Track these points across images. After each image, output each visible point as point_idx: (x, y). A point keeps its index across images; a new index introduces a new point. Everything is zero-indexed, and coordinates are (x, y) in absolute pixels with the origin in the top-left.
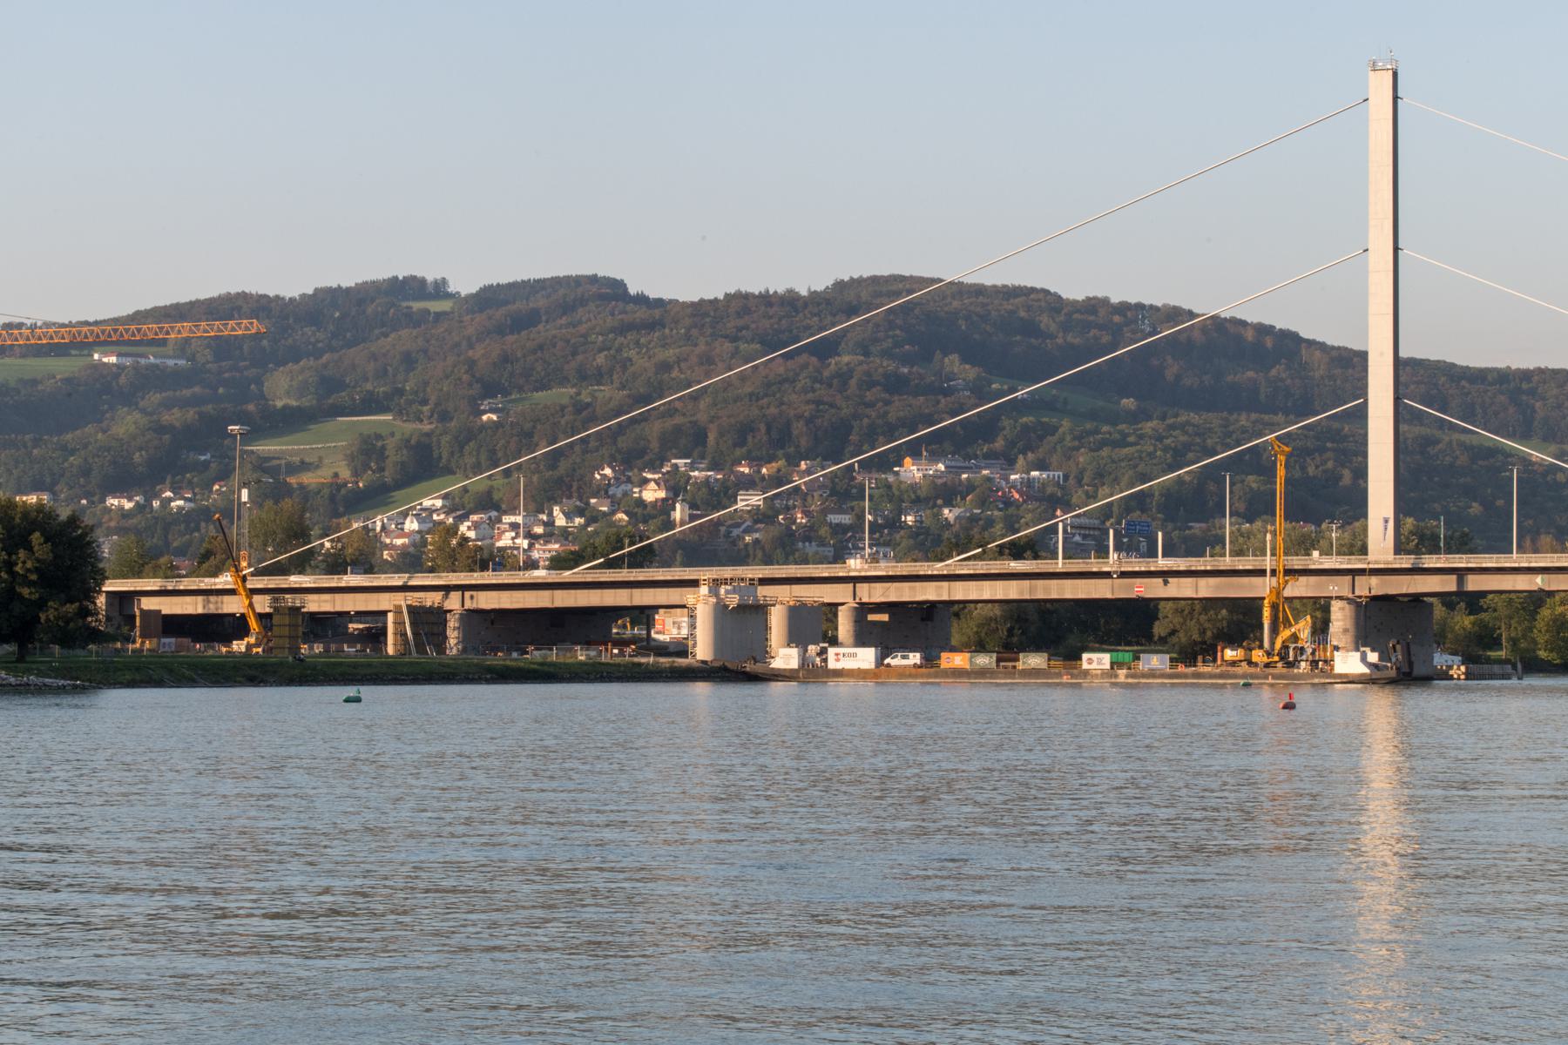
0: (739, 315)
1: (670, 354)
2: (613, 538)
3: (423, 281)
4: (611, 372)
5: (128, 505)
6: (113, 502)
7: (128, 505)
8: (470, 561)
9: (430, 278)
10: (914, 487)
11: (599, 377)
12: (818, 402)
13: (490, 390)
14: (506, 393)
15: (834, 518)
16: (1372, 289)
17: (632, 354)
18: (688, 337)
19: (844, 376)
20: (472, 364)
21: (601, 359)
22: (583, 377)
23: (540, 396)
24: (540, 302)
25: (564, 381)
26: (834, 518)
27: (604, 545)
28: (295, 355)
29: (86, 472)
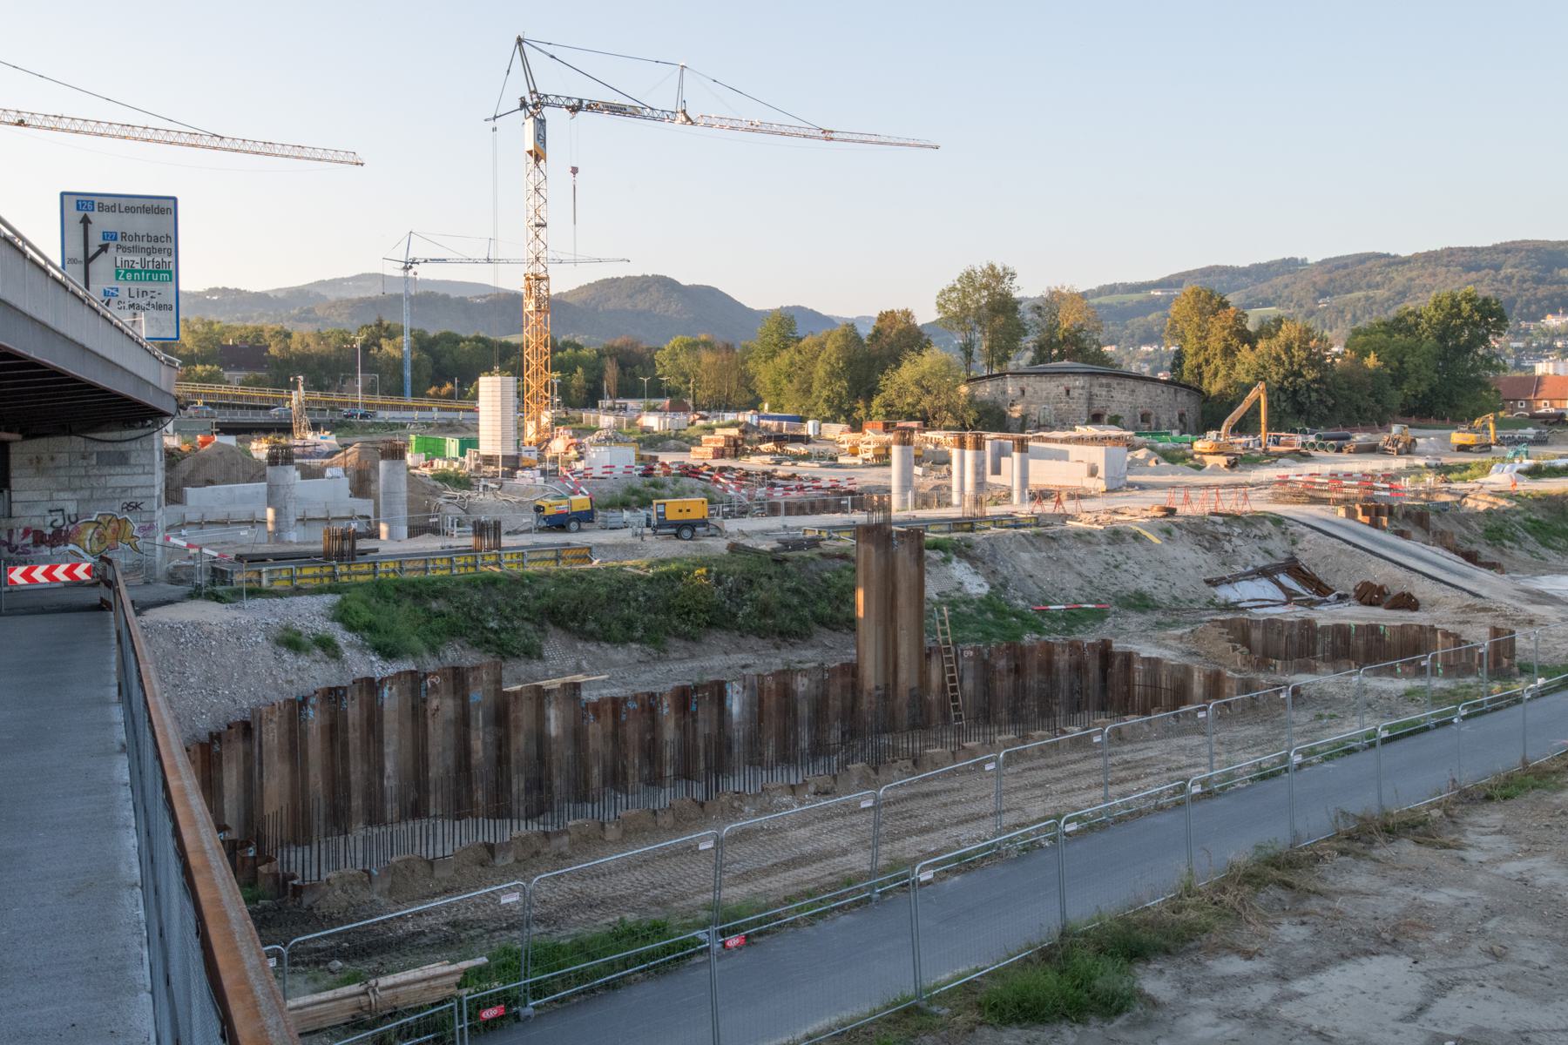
0: (1448, 256)
1: (1414, 274)
2: (1447, 302)
3: (1296, 259)
4: (1383, 284)
5: (1151, 349)
6: (1144, 348)
7: (1151, 349)
8: (1226, 332)
9: (1300, 258)
10: (1556, 328)
11: (1377, 286)
12: (1497, 290)
13: (1323, 294)
14: (1331, 296)
15: (1515, 345)
16: (226, 783)
17: (1395, 275)
18: (1423, 267)
19: (1509, 279)
20: (1315, 283)
21: (1378, 278)
22: (1369, 286)
23: (1349, 296)
24: (1349, 261)
25: (1360, 289)
26: (1515, 345)
27: (1432, 312)
28: (1238, 288)
29: (1132, 336)
